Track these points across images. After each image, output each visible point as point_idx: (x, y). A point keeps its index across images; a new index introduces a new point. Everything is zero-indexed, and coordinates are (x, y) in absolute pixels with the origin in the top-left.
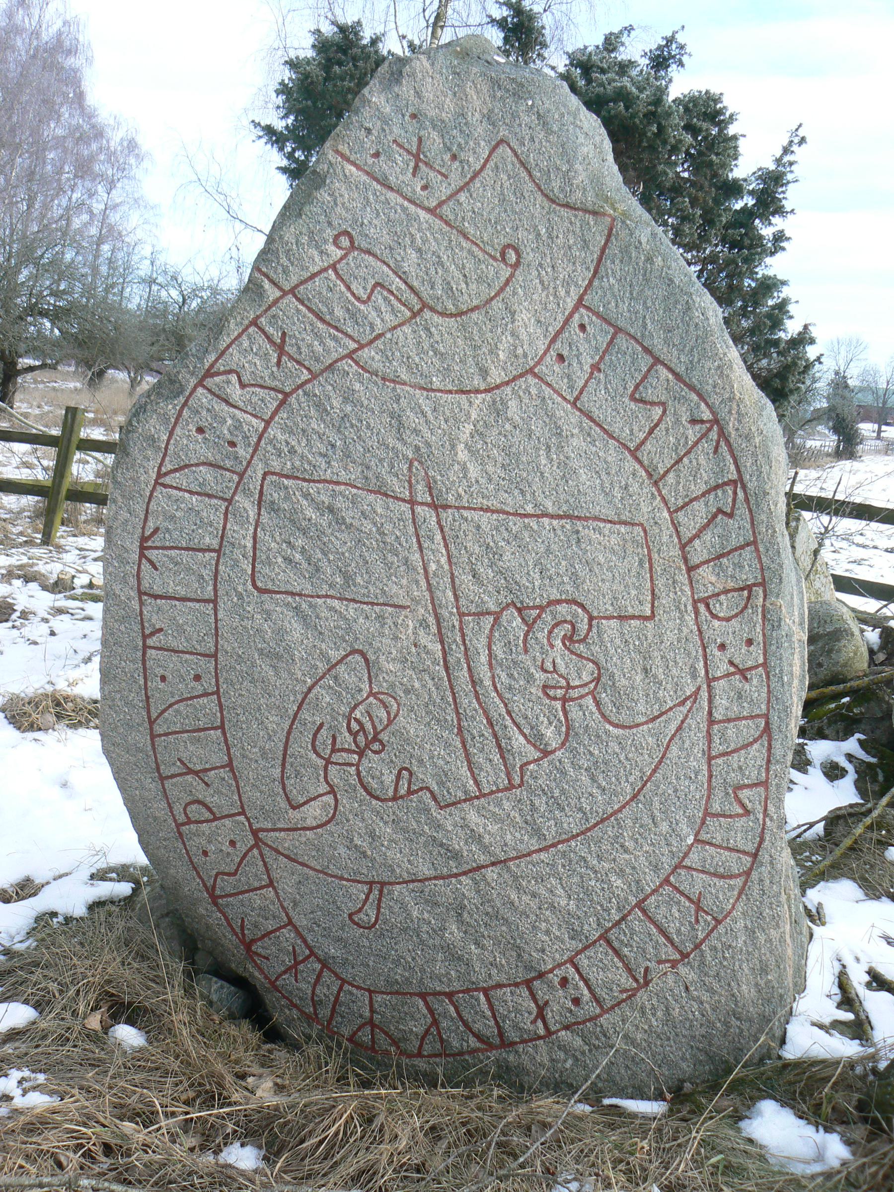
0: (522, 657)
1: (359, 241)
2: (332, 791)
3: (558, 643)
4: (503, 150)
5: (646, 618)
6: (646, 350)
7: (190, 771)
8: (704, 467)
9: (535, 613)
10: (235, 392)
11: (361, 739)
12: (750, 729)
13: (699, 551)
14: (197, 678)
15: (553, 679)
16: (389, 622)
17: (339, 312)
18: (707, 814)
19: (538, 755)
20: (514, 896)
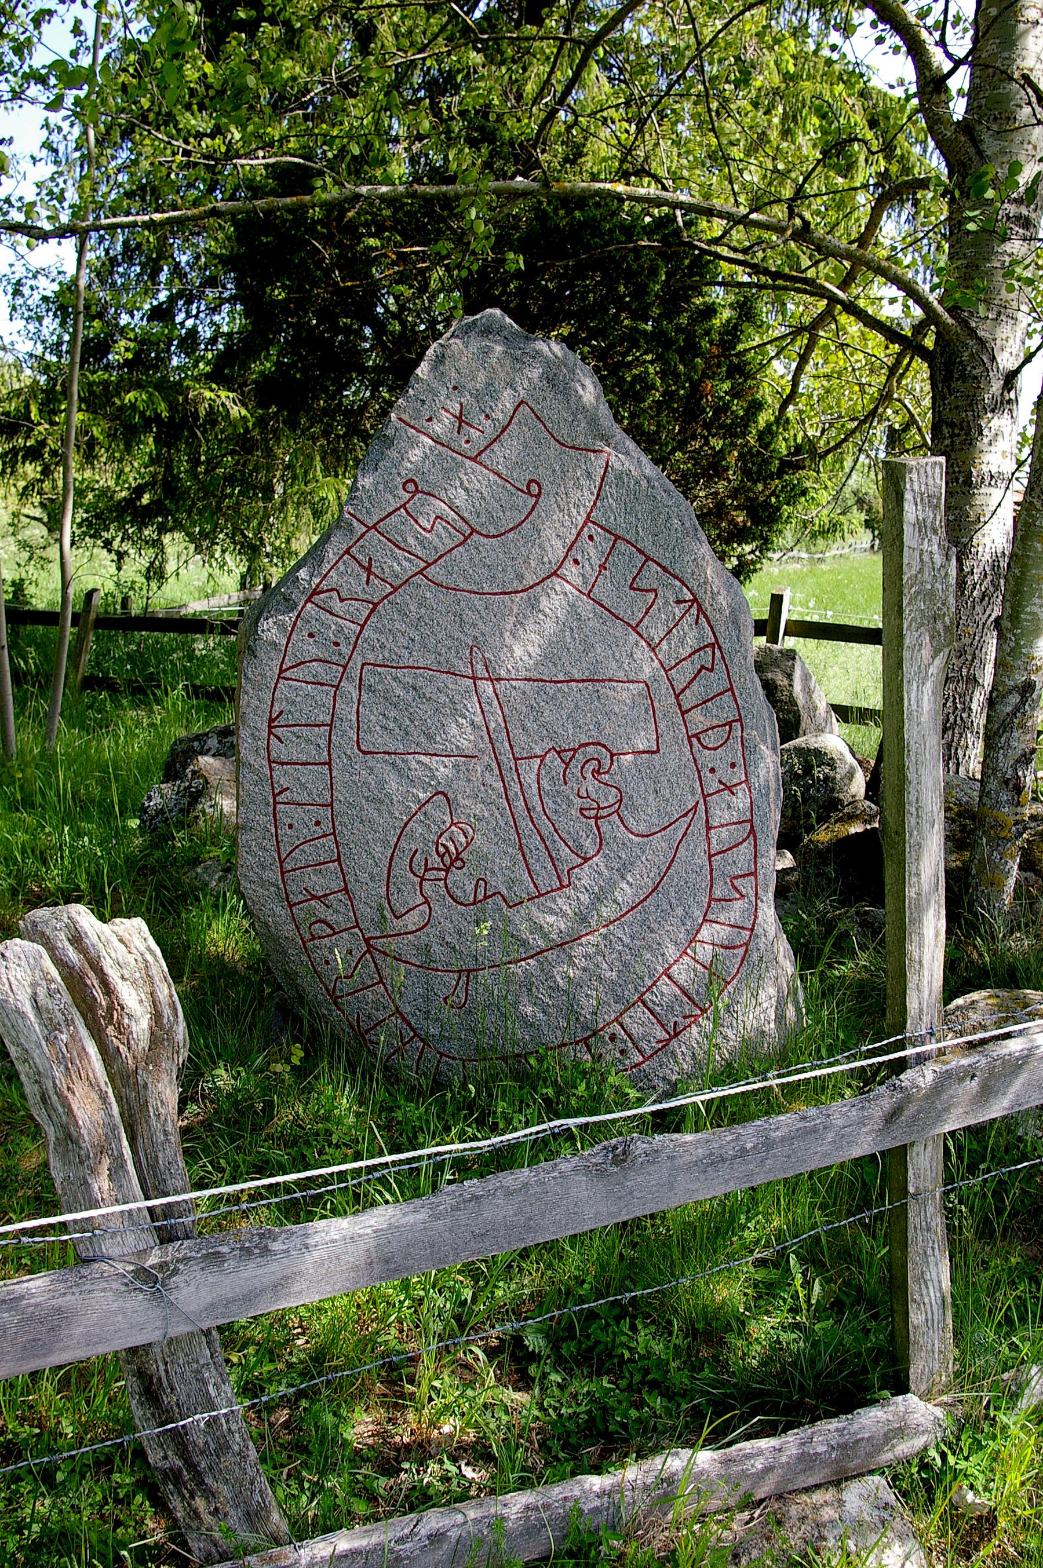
2: (427, 902)
3: (589, 775)
6: (639, 551)
7: (314, 897)
10: (337, 606)
11: (447, 858)
13: (689, 699)
14: (318, 823)
15: (587, 803)
17: (411, 540)
18: (711, 899)
19: (580, 861)
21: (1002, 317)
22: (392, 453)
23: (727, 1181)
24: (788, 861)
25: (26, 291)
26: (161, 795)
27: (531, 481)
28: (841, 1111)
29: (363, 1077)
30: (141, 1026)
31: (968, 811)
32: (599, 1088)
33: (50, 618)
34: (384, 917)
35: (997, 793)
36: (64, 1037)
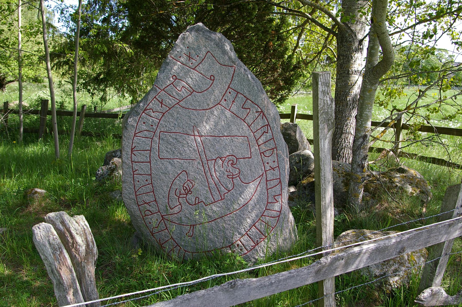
0: (222, 169)
1: (178, 77)
2: (180, 204)
3: (230, 165)
4: (209, 54)
5: (250, 158)
6: (245, 96)
7: (146, 203)
8: (260, 122)
9: (224, 158)
10: (152, 114)
11: (186, 191)
12: (276, 182)
13: (261, 141)
14: (147, 180)
15: (229, 174)
16: (191, 163)
17: (174, 94)
18: (268, 203)
19: (227, 191)
20: (224, 225)
21: (358, 23)
22: (169, 67)
23: (266, 293)
24: (292, 189)
25: (65, 12)
26: (102, 170)
27: (211, 75)
28: (304, 270)
29: (161, 258)
30: (83, 248)
31: (348, 174)
32: (234, 261)
33: (70, 114)
34: (167, 209)
35: (356, 169)
36: (58, 252)
